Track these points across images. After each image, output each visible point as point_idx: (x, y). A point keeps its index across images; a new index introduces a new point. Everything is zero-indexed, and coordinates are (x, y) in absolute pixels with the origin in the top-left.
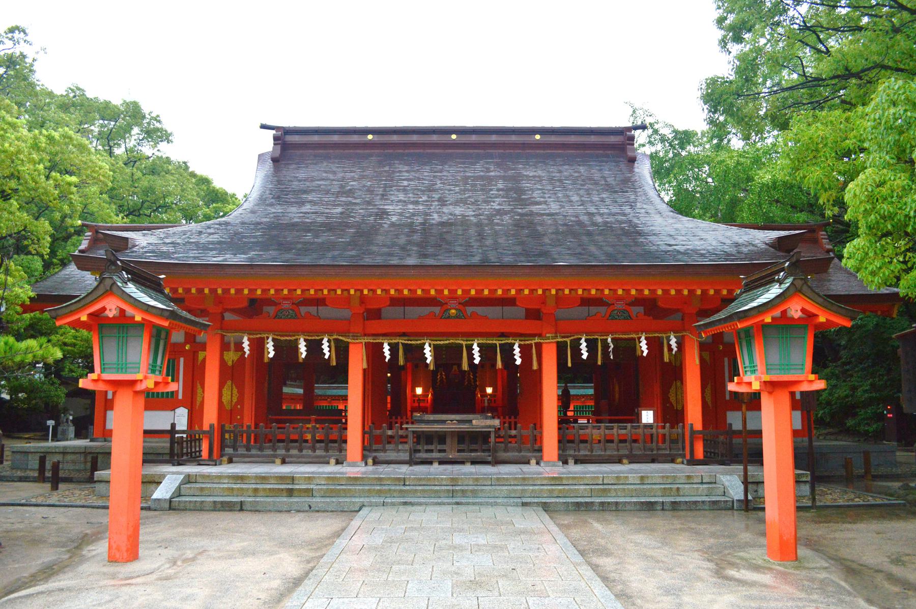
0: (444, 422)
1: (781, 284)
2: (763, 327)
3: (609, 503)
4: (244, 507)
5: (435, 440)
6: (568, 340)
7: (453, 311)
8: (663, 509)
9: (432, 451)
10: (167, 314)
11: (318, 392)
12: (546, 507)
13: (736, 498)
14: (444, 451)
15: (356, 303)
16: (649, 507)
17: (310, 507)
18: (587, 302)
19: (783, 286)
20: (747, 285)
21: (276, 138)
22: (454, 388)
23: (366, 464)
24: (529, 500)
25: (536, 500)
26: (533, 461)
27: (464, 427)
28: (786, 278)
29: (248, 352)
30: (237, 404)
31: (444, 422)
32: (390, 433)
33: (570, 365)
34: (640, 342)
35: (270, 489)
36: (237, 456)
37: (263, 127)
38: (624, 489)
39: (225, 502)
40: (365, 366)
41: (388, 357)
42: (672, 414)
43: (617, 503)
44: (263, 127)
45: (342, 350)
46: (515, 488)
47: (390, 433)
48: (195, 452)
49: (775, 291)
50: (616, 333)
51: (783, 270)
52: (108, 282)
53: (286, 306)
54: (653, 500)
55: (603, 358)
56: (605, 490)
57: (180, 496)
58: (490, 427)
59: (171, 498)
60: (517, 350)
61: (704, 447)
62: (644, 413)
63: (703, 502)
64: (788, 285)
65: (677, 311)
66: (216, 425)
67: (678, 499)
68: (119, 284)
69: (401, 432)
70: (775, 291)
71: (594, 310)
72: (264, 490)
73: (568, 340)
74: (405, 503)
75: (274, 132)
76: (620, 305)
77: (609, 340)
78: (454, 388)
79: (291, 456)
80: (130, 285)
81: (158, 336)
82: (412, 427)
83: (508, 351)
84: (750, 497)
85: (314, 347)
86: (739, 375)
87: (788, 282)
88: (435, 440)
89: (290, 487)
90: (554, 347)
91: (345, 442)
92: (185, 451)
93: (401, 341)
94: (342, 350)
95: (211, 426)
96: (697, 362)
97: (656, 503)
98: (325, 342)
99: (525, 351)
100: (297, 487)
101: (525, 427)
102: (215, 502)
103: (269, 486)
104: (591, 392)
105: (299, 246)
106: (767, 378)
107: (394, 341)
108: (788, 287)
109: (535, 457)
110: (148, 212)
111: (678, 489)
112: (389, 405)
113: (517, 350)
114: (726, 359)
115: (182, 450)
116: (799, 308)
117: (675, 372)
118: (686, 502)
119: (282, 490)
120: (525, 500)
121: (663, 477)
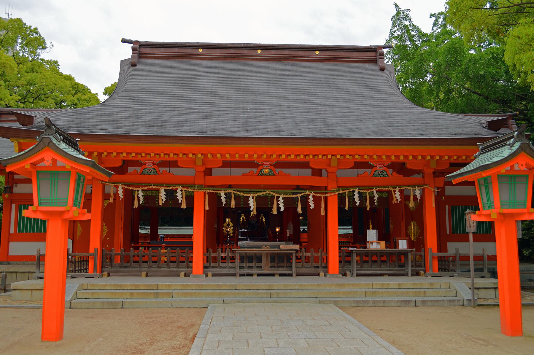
0: (260, 247)
1: (511, 147)
2: (500, 177)
3: (378, 301)
4: (124, 306)
5: (255, 261)
6: (347, 192)
7: (267, 170)
8: (416, 306)
9: (252, 267)
10: (91, 163)
11: (160, 232)
12: (335, 303)
13: (466, 298)
14: (261, 267)
15: (199, 163)
16: (406, 303)
17: (172, 305)
18: (358, 165)
19: (513, 148)
20: (482, 149)
21: (134, 49)
22: (264, 225)
23: (207, 276)
24: (324, 299)
25: (329, 299)
26: (322, 274)
27: (276, 250)
28: (514, 142)
29: (122, 197)
30: (106, 237)
31: (260, 247)
32: (223, 254)
33: (347, 208)
34: (395, 194)
35: (142, 293)
36: (113, 272)
37: (124, 41)
38: (388, 292)
39: (111, 302)
40: (207, 208)
41: (224, 203)
42: (417, 244)
43: (384, 301)
44: (124, 41)
45: (190, 199)
46: (314, 291)
47: (223, 254)
48: (83, 270)
49: (505, 152)
50: (379, 186)
51: (513, 137)
52: (46, 141)
53: (150, 166)
54: (409, 299)
55: (370, 206)
56: (375, 292)
57: (76, 298)
58: (292, 250)
59: (71, 300)
60: (311, 199)
61: (439, 265)
62: (400, 242)
63: (443, 301)
64: (517, 147)
65: (418, 172)
66: (99, 250)
67: (426, 299)
68: (54, 142)
69: (230, 254)
70: (505, 152)
71: (361, 171)
72: (138, 293)
73: (347, 192)
74: (239, 302)
75: (132, 45)
76: (380, 167)
77: (375, 192)
78: (264, 225)
79: (153, 271)
80: (63, 143)
81: (80, 179)
82: (239, 251)
83: (305, 199)
84: (476, 298)
85: (171, 194)
86: (479, 210)
87: (517, 145)
88: (255, 261)
89: (156, 291)
90: (336, 198)
91: (191, 262)
92: (77, 269)
93: (232, 191)
94: (190, 199)
95: (96, 250)
96: (434, 205)
97: (411, 301)
98: (179, 191)
99: (317, 200)
100: (162, 291)
101: (317, 251)
102: (103, 302)
103: (141, 291)
104: (351, 232)
105: (160, 124)
106: (501, 211)
107: (227, 191)
108: (518, 149)
109: (323, 271)
110: (31, 100)
111: (425, 292)
112: (216, 239)
113: (311, 199)
114: (447, 207)
115: (75, 268)
116: (524, 163)
117: (417, 216)
118: (432, 301)
119: (151, 293)
120: (321, 299)
121: (414, 284)
